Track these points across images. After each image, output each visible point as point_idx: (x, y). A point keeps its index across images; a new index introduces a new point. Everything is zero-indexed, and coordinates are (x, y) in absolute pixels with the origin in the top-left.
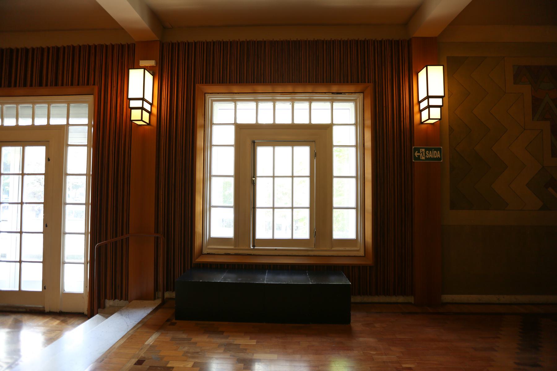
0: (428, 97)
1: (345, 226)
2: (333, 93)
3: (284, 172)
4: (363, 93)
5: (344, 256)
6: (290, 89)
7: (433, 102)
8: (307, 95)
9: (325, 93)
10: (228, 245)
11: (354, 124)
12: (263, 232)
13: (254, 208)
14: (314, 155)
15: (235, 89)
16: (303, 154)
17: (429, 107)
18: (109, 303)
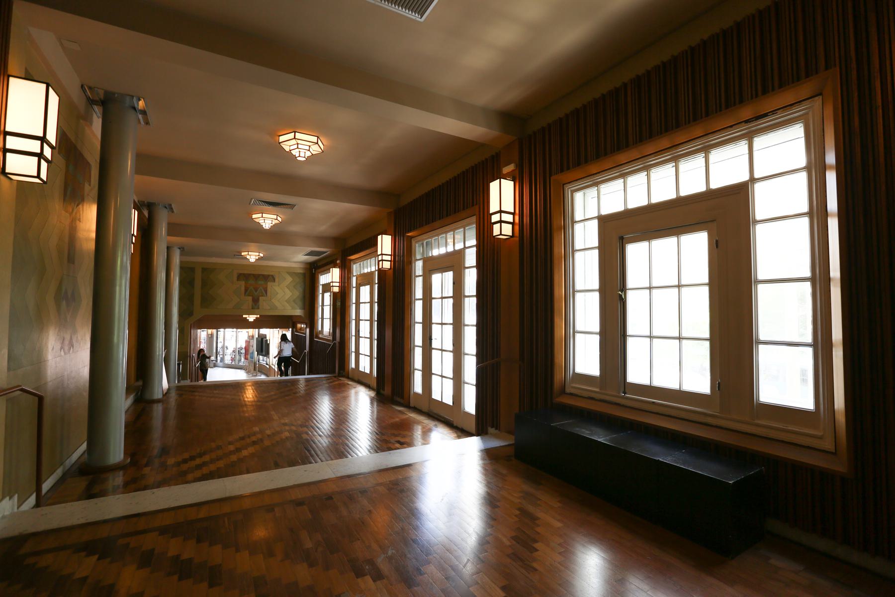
0: (501, 212)
1: (786, 379)
2: (747, 122)
3: (671, 278)
4: (820, 94)
5: (783, 442)
6: (664, 142)
7: (385, 258)
8: (699, 142)
9: (731, 126)
10: (590, 386)
11: (804, 168)
12: (636, 374)
13: (624, 336)
14: (715, 247)
15: (593, 168)
16: (696, 247)
17: (382, 260)
18: (491, 430)
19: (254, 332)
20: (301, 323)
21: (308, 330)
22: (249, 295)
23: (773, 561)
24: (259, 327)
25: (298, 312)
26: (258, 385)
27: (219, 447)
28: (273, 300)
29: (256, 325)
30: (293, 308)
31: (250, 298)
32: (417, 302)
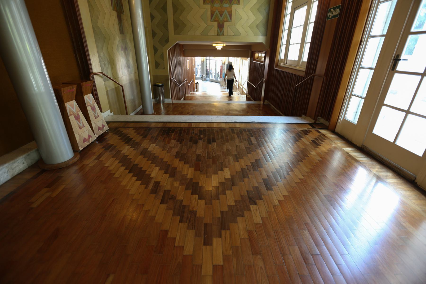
18: (303, 116)
19: (225, 60)
20: (260, 52)
21: (267, 60)
22: (215, 21)
23: (122, 75)
24: (228, 56)
25: (260, 39)
26: (194, 91)
27: (288, 174)
28: (237, 26)
29: (227, 52)
30: (256, 35)
31: (216, 24)
32: (283, 46)
